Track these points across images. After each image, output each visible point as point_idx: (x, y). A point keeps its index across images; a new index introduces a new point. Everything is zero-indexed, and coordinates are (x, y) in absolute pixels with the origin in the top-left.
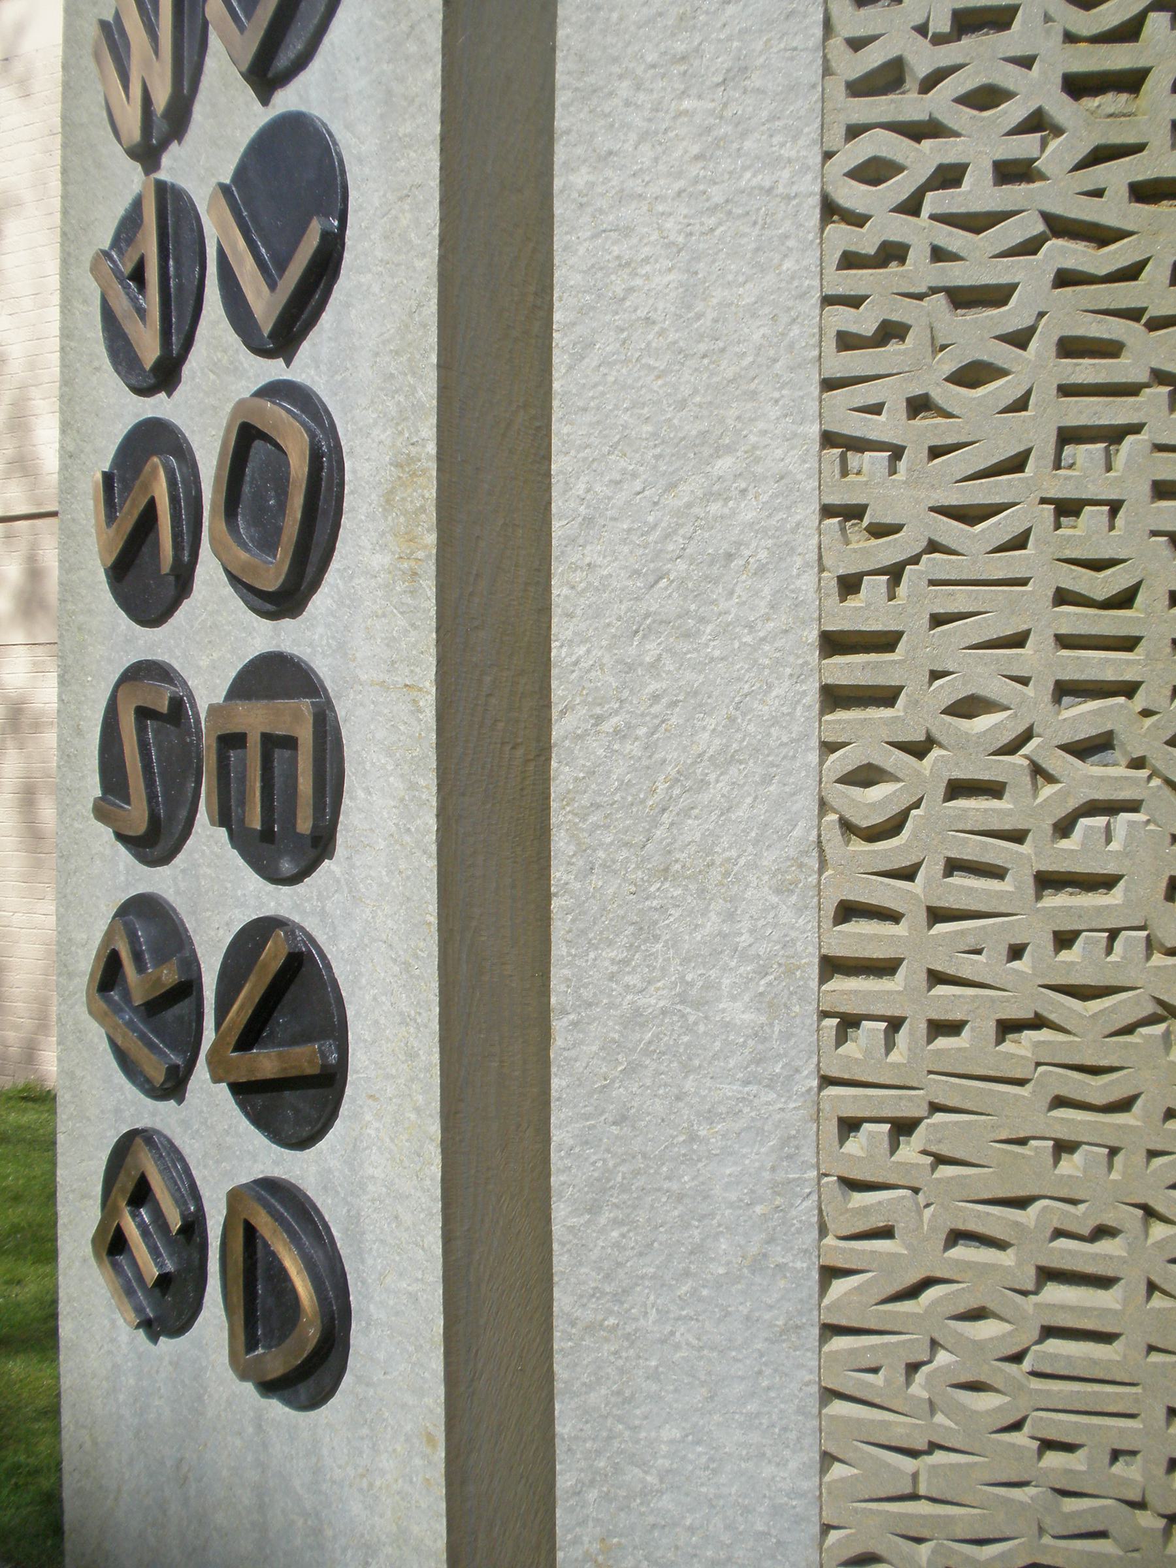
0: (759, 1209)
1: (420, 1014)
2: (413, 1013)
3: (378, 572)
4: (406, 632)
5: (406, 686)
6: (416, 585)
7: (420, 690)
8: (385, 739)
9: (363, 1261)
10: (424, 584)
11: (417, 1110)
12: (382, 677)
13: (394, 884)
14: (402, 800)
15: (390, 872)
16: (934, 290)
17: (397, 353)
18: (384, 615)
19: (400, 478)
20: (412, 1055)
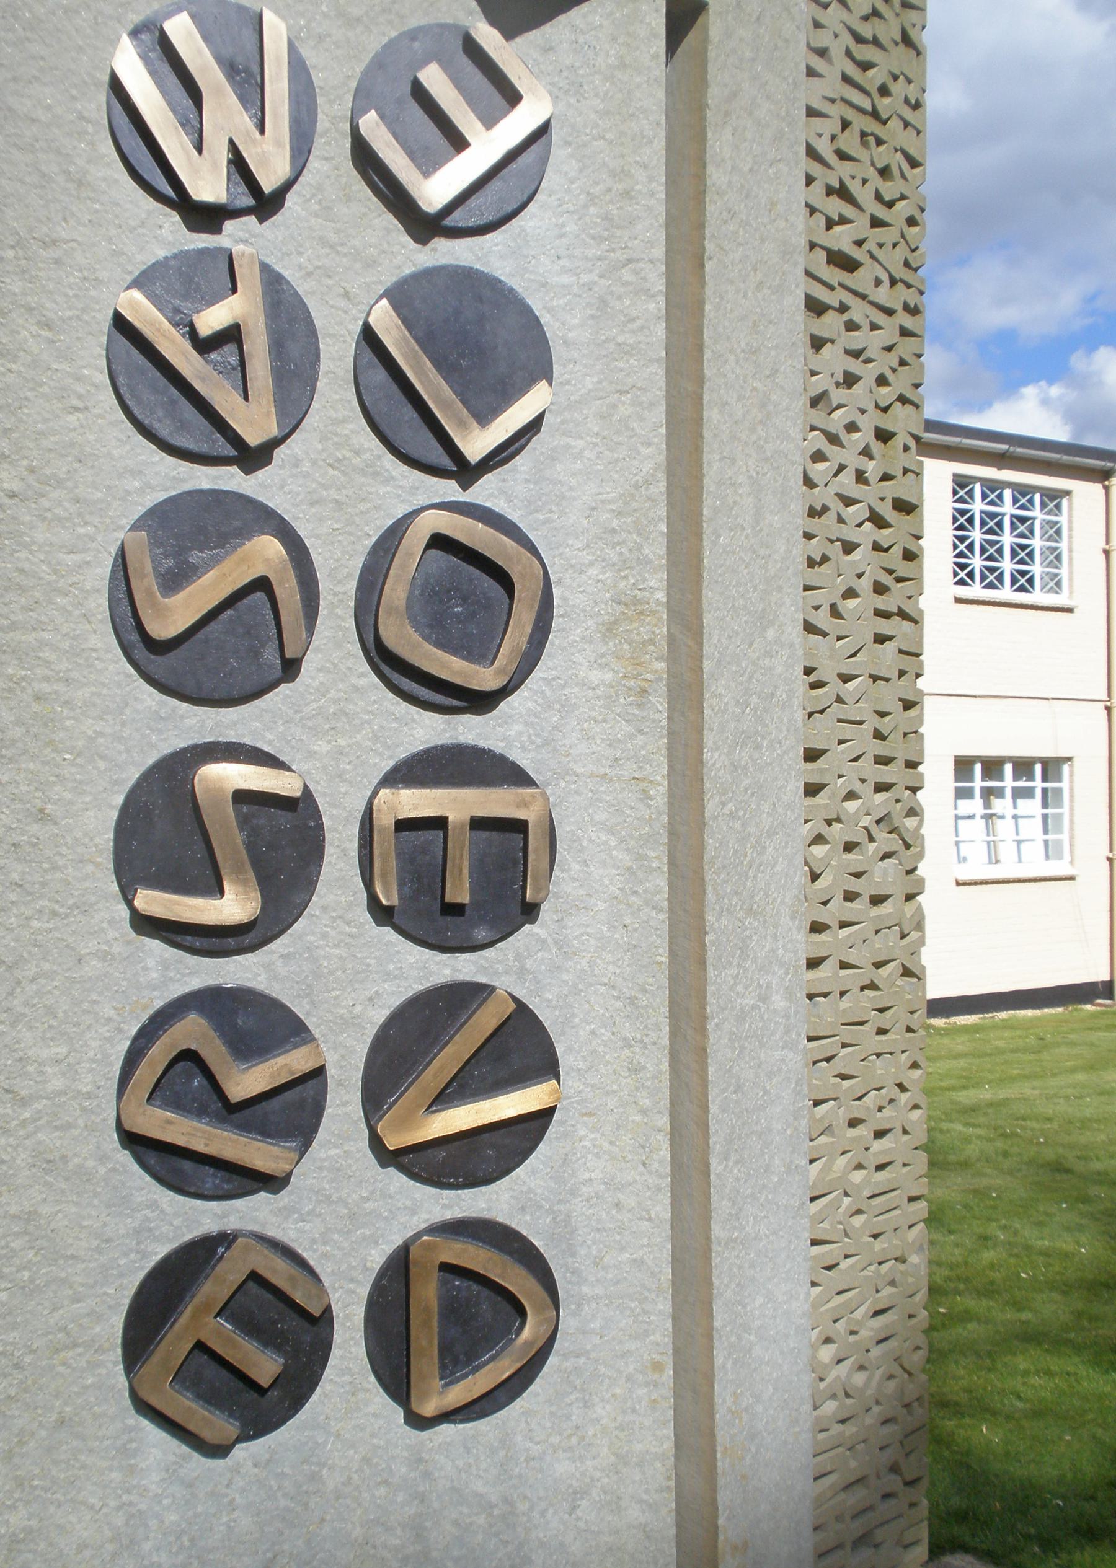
0: (788, 1132)
1: (647, 1035)
2: (638, 1036)
3: (598, 685)
4: (632, 736)
5: (634, 778)
6: (644, 700)
7: (651, 782)
8: (607, 820)
9: (573, 1255)
10: (654, 700)
11: (644, 1112)
12: (602, 771)
13: (617, 936)
14: (629, 869)
15: (612, 928)
16: (838, 540)
17: (619, 513)
18: (605, 721)
19: (624, 613)
20: (635, 1069)
